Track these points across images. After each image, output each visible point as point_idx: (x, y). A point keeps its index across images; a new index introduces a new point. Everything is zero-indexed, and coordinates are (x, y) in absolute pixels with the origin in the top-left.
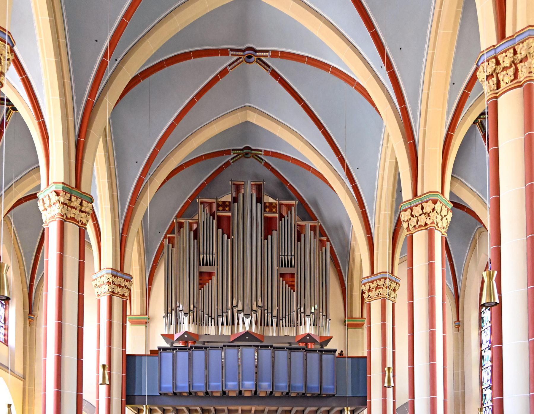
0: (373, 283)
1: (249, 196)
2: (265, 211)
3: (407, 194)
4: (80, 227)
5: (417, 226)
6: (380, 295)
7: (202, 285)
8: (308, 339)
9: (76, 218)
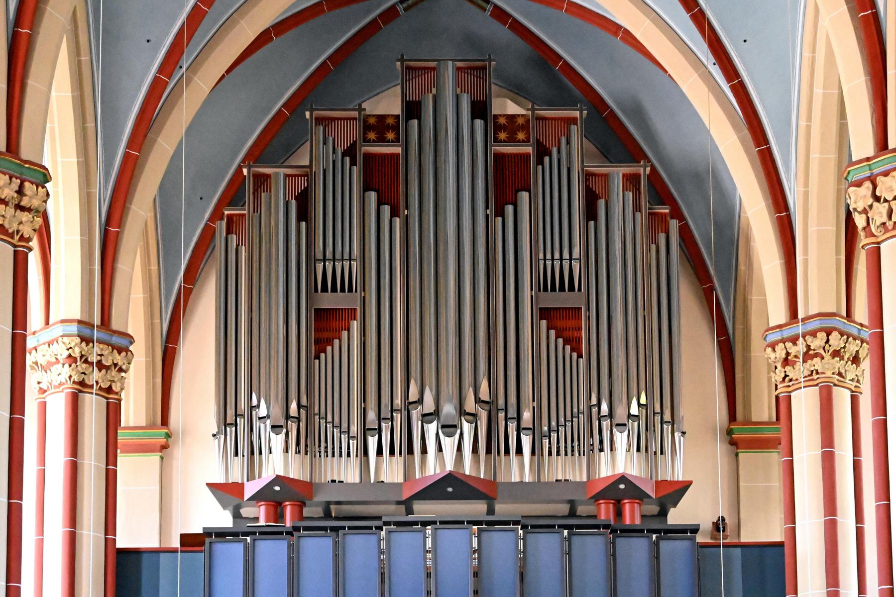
0: (795, 343)
1: (450, 100)
2: (496, 140)
3: (862, 143)
4: (15, 246)
5: (890, 225)
6: (815, 376)
7: (321, 344)
8: (620, 491)
9: (7, 225)
